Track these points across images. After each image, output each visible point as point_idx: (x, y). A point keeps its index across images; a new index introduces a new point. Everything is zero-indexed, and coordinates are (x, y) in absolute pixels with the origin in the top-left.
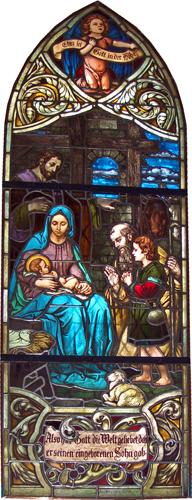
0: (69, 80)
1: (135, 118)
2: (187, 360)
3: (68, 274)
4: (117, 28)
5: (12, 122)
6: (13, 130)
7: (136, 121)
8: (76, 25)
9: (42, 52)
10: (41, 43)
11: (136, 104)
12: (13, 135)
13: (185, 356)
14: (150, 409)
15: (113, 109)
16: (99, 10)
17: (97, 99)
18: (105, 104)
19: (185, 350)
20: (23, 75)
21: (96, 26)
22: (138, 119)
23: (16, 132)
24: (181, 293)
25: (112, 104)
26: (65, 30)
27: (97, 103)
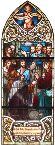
0: (19, 26)
1: (39, 36)
2: (53, 58)
3: (32, 41)
4: (33, 9)
5: (3, 40)
6: (4, 42)
7: (39, 37)
8: (22, 9)
9: (12, 18)
10: (18, 8)
11: (39, 32)
12: (4, 44)
13: (53, 56)
14: (43, 121)
15: (32, 34)
16: (27, 4)
17: (28, 32)
18: (30, 33)
19: (52, 143)
20: (6, 25)
21: (28, 8)
22: (40, 37)
23: (4, 43)
24: (52, 68)
25: (32, 33)
26: (18, 11)
27: (28, 33)
